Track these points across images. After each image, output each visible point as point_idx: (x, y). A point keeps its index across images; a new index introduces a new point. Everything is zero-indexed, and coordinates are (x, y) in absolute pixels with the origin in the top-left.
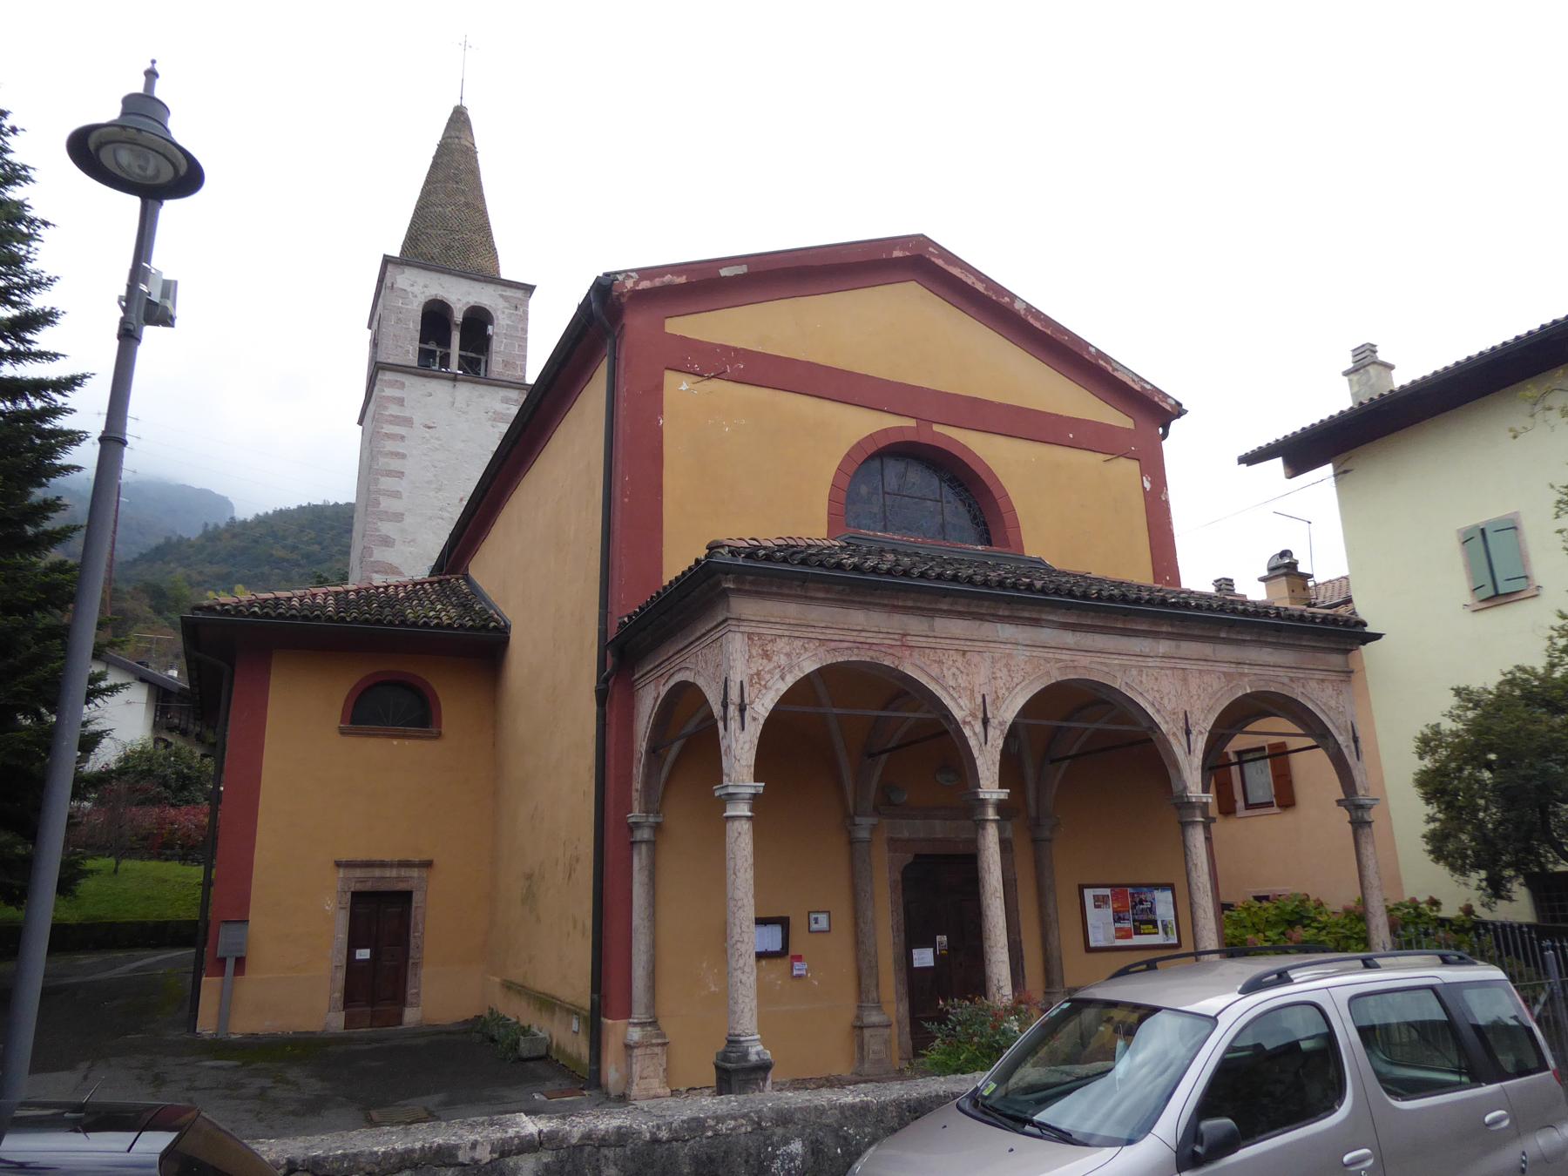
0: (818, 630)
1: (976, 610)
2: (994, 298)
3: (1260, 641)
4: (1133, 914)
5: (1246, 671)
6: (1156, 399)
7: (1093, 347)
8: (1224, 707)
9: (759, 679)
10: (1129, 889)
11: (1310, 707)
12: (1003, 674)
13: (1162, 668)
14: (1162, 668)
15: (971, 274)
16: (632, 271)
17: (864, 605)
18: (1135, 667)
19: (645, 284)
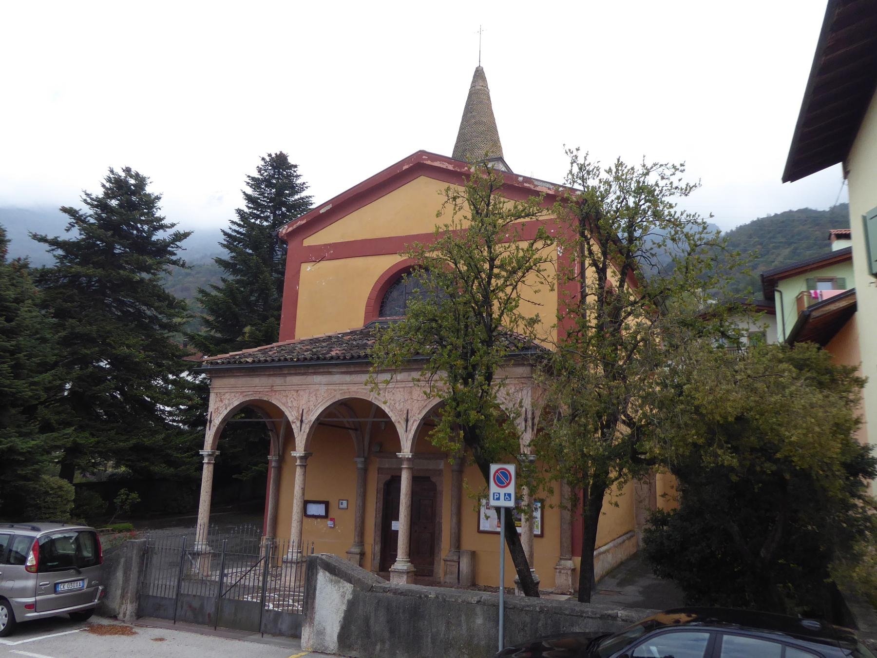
2: (459, 170)
7: (521, 176)
12: (313, 399)
17: (258, 376)
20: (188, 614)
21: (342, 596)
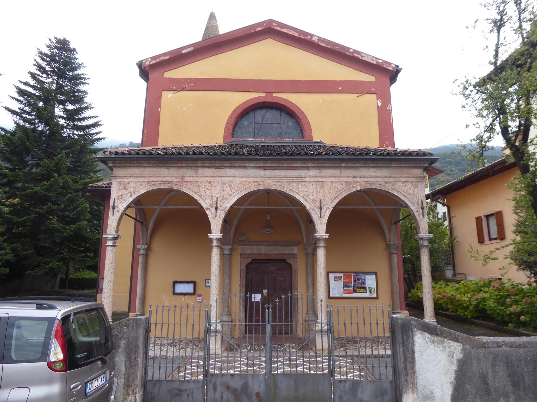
0: (147, 178)
1: (214, 165)
2: (303, 38)
3: (232, 166)
4: (354, 284)
5: (359, 180)
6: (384, 66)
8: (343, 197)
9: (122, 197)
10: (352, 274)
11: (396, 194)
13: (310, 182)
14: (310, 182)
15: (292, 30)
16: (149, 58)
18: (295, 182)
19: (154, 62)
20: (225, 396)
21: (449, 356)
